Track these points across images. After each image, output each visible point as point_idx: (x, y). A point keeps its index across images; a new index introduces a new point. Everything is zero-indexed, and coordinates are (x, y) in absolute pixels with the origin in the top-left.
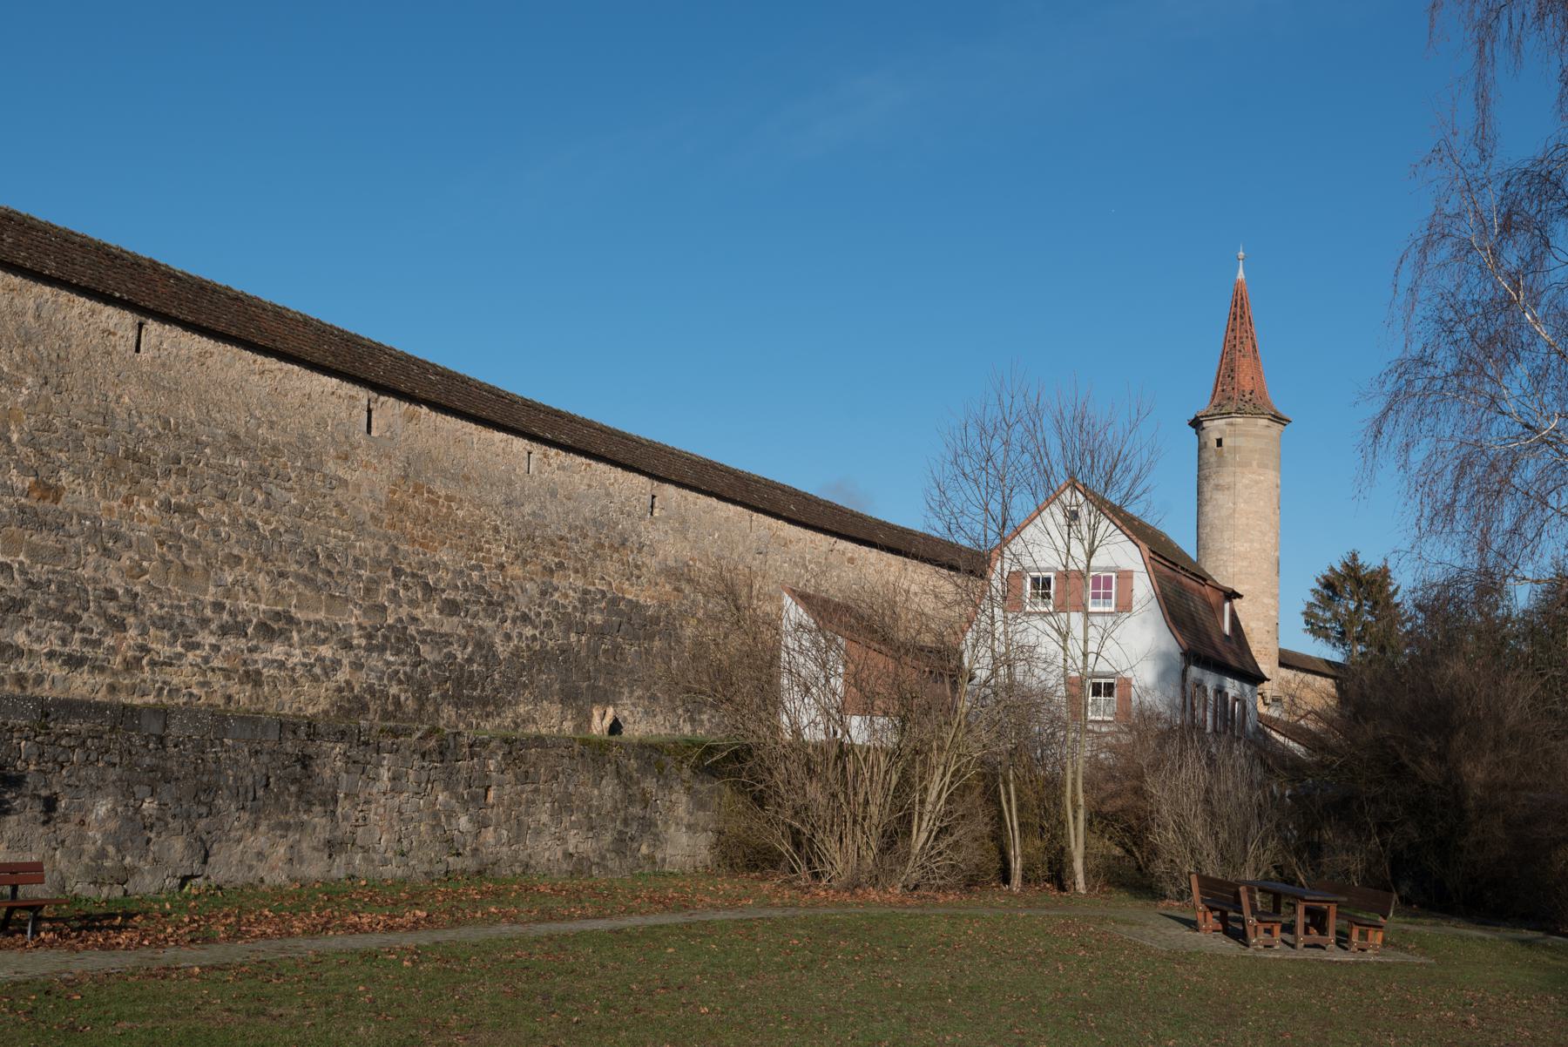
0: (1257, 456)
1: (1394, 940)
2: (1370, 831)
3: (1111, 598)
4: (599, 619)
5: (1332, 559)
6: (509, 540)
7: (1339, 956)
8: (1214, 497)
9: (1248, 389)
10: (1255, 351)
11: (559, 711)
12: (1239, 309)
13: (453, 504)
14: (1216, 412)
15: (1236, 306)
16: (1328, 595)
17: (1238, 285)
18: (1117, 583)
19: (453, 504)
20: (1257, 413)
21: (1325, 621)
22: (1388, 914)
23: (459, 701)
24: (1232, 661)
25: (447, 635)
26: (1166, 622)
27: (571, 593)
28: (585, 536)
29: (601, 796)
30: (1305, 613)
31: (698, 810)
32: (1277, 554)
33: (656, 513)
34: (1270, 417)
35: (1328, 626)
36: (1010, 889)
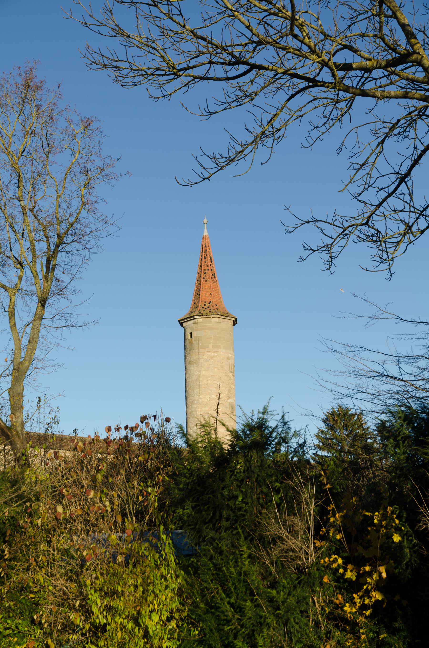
0: (212, 341)
17: (204, 238)
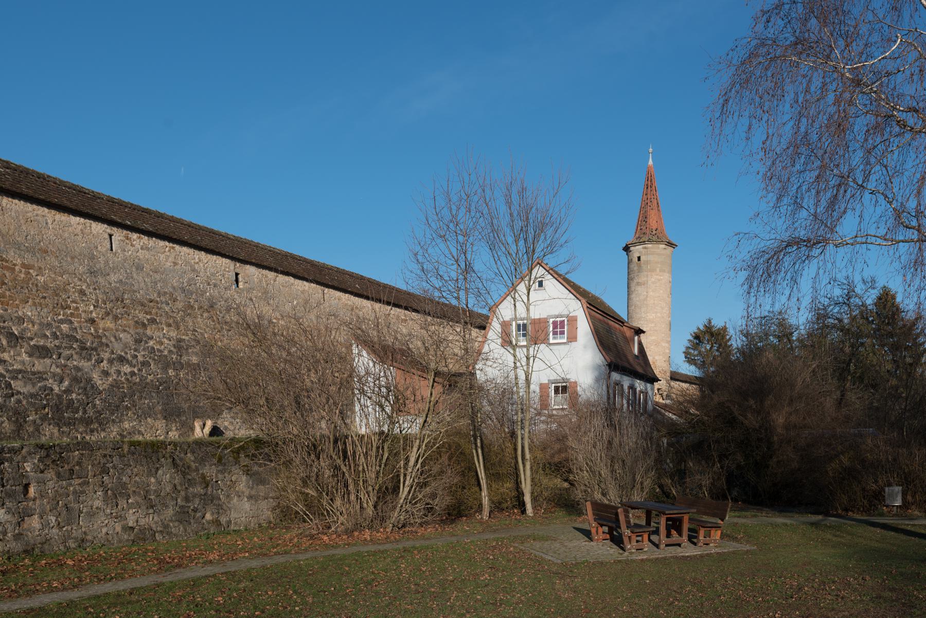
0: (659, 266)
1: (728, 533)
2: (714, 460)
4: (194, 360)
5: (699, 324)
6: (97, 301)
7: (688, 550)
11: (164, 425)
13: (31, 271)
17: (649, 168)
19: (31, 271)
20: (659, 241)
21: (695, 356)
22: (725, 518)
23: (59, 422)
24: (640, 370)
25: (39, 372)
26: (598, 346)
27: (166, 341)
28: (175, 300)
29: (159, 483)
30: (684, 352)
31: (257, 485)
32: (670, 319)
33: (241, 285)
35: (696, 358)
36: (482, 518)
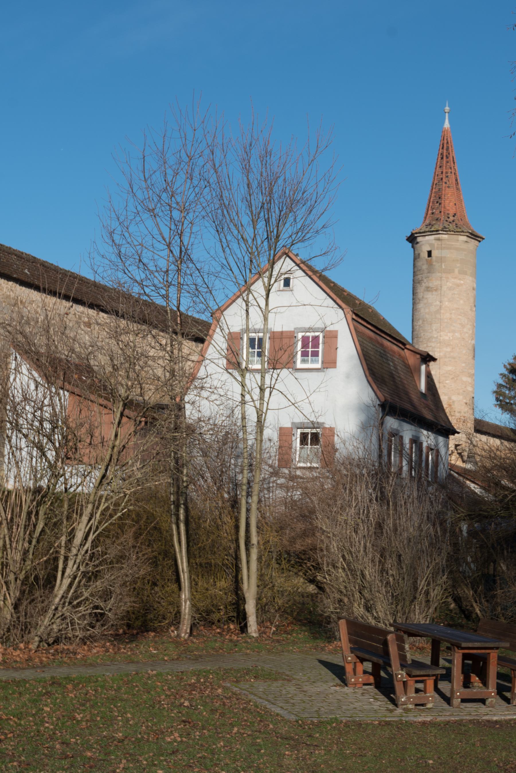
0: (458, 265)
3: (318, 356)
8: (425, 297)
9: (451, 213)
10: (457, 184)
12: (445, 151)
14: (427, 230)
15: (443, 148)
16: (513, 378)
18: (324, 343)
20: (458, 231)
24: (428, 415)
30: (495, 392)
34: (467, 234)
35: (512, 402)
